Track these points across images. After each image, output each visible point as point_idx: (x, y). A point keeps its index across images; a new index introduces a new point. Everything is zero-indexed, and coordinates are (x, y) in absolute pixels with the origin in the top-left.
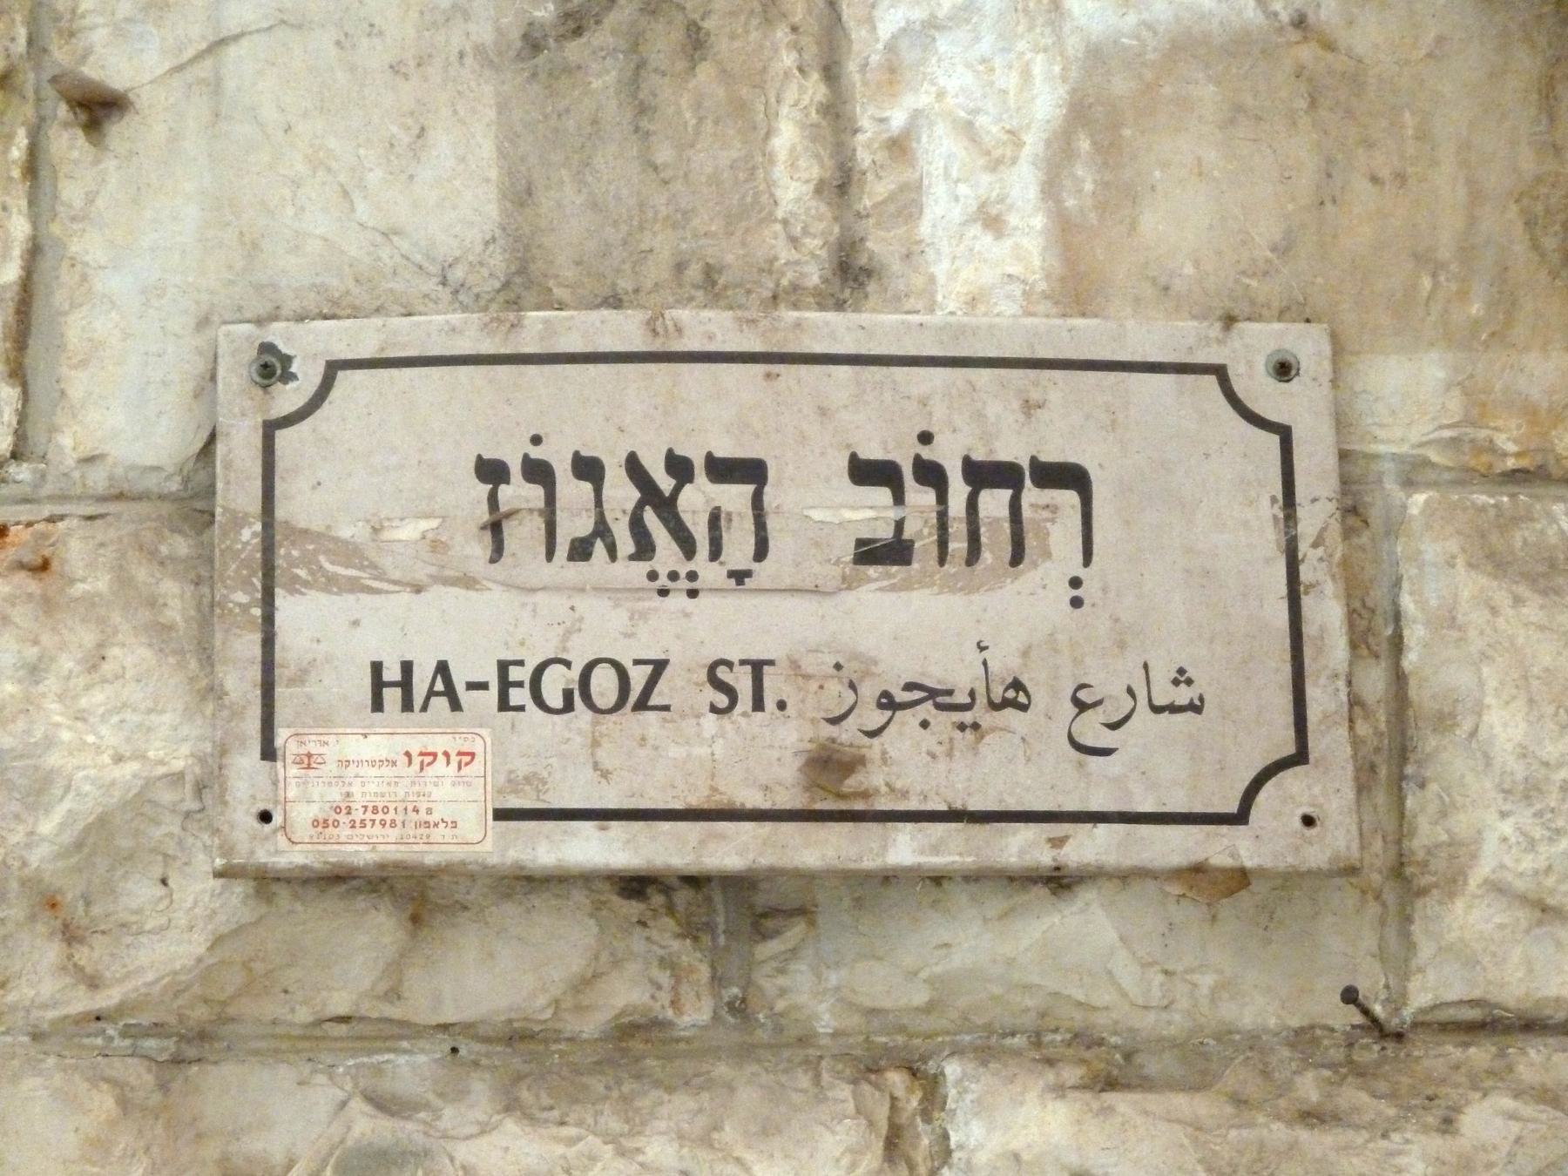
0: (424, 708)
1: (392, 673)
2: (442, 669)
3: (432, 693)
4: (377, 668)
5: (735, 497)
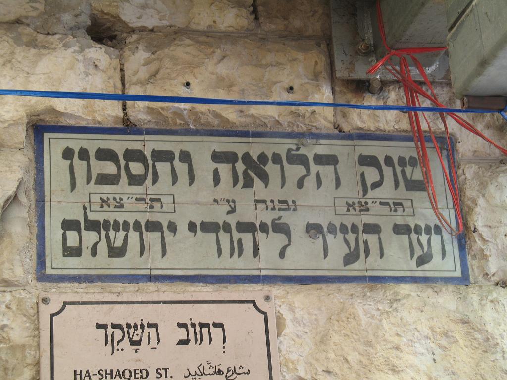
0: (84, 379)
1: (78, 372)
2: (88, 371)
3: (85, 376)
4: (75, 371)
5: (153, 331)
